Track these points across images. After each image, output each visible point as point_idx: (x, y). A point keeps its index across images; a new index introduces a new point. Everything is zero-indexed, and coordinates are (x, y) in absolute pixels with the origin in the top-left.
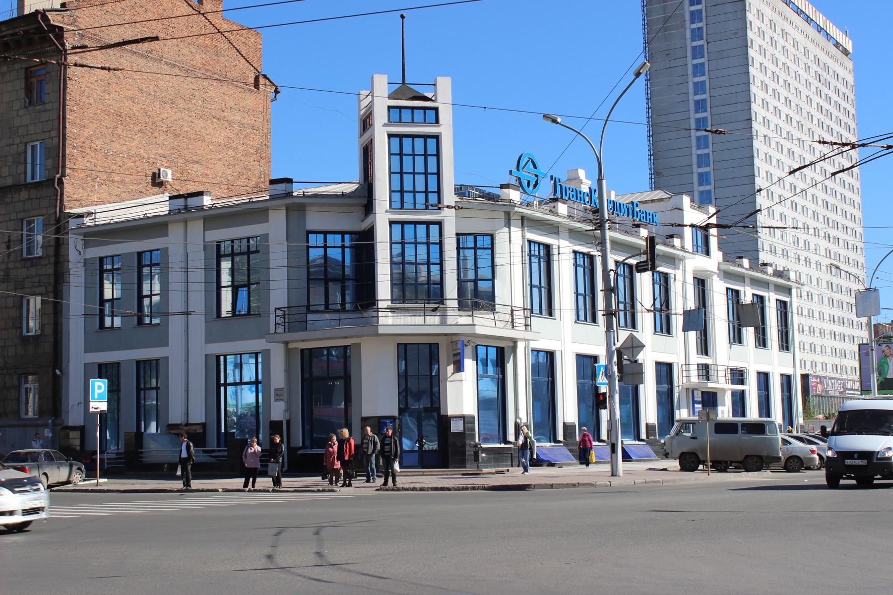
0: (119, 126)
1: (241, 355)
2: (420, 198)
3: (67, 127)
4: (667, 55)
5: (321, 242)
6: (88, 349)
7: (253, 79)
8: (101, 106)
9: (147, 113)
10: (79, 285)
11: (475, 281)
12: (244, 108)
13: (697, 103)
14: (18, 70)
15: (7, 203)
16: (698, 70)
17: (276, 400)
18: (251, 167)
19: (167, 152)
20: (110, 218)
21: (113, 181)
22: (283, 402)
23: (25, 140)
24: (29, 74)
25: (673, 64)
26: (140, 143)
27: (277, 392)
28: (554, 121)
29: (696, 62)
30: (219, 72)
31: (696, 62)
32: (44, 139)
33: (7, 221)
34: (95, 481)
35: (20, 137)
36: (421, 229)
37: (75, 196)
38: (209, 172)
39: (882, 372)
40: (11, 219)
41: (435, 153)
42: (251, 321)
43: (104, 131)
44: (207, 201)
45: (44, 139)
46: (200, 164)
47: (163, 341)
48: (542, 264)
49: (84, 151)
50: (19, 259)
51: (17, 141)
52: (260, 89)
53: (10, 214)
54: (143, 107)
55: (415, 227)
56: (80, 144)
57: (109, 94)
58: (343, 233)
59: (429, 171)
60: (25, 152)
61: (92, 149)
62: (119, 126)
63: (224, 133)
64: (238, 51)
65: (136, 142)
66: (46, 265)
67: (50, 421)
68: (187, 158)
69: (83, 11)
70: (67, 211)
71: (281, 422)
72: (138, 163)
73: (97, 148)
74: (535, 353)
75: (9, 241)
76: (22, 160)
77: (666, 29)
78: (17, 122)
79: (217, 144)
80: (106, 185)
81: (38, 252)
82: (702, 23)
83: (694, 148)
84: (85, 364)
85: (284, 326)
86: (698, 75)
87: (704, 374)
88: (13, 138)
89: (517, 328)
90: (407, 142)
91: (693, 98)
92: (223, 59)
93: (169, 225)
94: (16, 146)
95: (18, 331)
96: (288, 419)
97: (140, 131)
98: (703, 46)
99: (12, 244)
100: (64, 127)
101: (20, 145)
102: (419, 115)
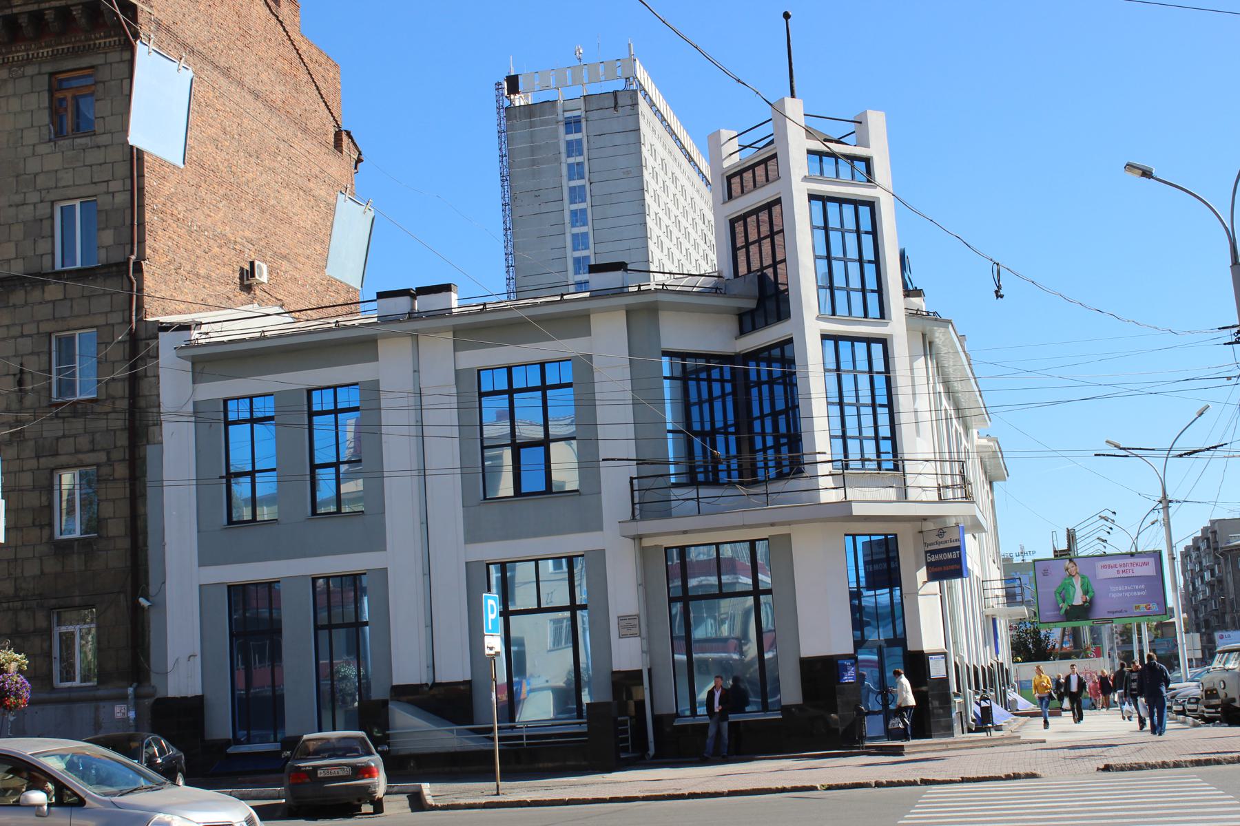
3: (146, 175)
4: (536, 196)
7: (333, 134)
10: (601, 403)
14: (32, 77)
15: (14, 306)
16: (578, 217)
17: (621, 636)
20: (260, 330)
21: (198, 275)
23: (52, 197)
24: (55, 85)
25: (544, 208)
27: (623, 623)
28: (1147, 174)
29: (574, 207)
31: (574, 207)
32: (95, 196)
33: (15, 338)
34: (493, 785)
35: (40, 191)
39: (1067, 596)
43: (187, 189)
44: (454, 300)
45: (95, 196)
47: (377, 542)
49: (165, 218)
50: (44, 403)
51: (33, 197)
52: (344, 153)
55: (853, 346)
60: (52, 217)
64: (318, 88)
65: (221, 214)
66: (107, 413)
67: (130, 690)
70: (149, 319)
71: (640, 672)
73: (179, 216)
75: (22, 372)
77: (534, 163)
78: (33, 166)
80: (190, 280)
81: (85, 388)
82: (582, 157)
84: (200, 586)
86: (578, 224)
88: (25, 193)
93: (379, 341)
94: (31, 207)
95: (46, 532)
97: (225, 196)
98: (584, 186)
99: (28, 378)
100: (141, 176)
101: (40, 206)
102: (845, 167)
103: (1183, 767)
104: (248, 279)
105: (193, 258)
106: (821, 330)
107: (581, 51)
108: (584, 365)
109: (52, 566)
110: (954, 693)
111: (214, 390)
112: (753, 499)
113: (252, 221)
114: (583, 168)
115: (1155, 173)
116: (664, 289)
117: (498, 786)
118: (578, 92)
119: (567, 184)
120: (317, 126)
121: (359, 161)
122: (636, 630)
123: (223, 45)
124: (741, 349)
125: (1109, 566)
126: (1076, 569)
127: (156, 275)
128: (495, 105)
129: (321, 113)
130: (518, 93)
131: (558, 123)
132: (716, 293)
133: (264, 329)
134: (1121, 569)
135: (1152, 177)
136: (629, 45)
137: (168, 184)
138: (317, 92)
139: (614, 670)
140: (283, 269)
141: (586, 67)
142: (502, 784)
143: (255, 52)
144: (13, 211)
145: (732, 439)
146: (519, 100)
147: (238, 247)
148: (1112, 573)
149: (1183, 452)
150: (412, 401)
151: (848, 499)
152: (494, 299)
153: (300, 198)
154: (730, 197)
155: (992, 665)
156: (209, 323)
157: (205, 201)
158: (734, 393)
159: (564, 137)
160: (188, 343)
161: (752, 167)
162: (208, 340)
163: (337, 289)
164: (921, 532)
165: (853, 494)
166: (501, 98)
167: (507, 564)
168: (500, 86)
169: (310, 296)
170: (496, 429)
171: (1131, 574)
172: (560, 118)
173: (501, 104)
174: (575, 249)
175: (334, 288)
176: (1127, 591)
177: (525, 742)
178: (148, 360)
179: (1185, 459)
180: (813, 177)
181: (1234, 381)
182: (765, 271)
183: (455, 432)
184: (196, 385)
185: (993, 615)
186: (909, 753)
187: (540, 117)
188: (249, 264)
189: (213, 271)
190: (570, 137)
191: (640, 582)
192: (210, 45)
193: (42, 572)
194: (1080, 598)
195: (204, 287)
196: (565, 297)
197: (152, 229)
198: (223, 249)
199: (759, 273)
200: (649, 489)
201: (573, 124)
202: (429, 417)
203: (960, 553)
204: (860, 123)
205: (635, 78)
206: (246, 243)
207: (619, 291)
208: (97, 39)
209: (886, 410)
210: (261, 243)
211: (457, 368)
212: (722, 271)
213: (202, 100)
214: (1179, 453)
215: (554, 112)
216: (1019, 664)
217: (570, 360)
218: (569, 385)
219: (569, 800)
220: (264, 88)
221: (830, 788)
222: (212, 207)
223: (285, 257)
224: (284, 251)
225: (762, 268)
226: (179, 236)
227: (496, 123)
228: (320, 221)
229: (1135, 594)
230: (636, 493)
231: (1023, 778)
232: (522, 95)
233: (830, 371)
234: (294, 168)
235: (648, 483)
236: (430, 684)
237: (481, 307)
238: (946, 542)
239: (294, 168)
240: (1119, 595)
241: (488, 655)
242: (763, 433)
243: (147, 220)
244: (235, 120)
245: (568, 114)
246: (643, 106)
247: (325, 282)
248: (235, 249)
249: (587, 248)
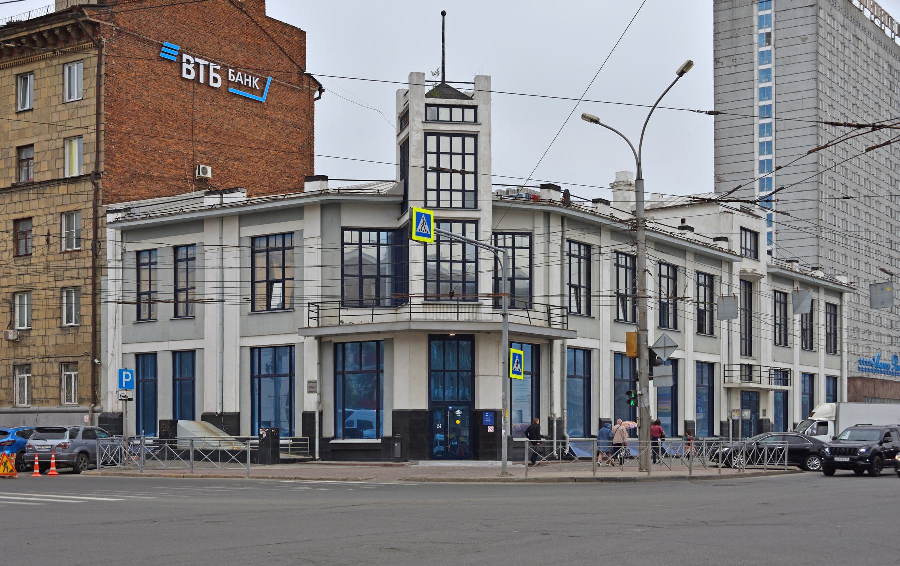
2: (458, 196)
5: (356, 239)
9: (187, 110)
11: (513, 280)
17: (309, 392)
18: (294, 165)
19: (207, 149)
20: (180, 209)
22: (316, 395)
27: (310, 385)
36: (457, 229)
37: (114, 191)
38: (250, 170)
40: (51, 213)
48: (582, 265)
50: (59, 252)
53: (49, 208)
54: (182, 104)
57: (148, 91)
58: (379, 231)
59: (467, 170)
62: (158, 123)
63: (266, 132)
68: (228, 155)
69: (121, 7)
71: (313, 414)
72: (177, 160)
74: (700, 365)
76: (61, 156)
79: (258, 142)
83: (757, 154)
85: (318, 320)
87: (748, 375)
89: (554, 327)
90: (445, 141)
92: (265, 58)
109: (61, 340)
110: (324, 441)
115: (601, 122)
116: (339, 192)
144: (47, 144)
193: (57, 344)
208: (83, 44)
220: (225, 56)
249: (770, 99)
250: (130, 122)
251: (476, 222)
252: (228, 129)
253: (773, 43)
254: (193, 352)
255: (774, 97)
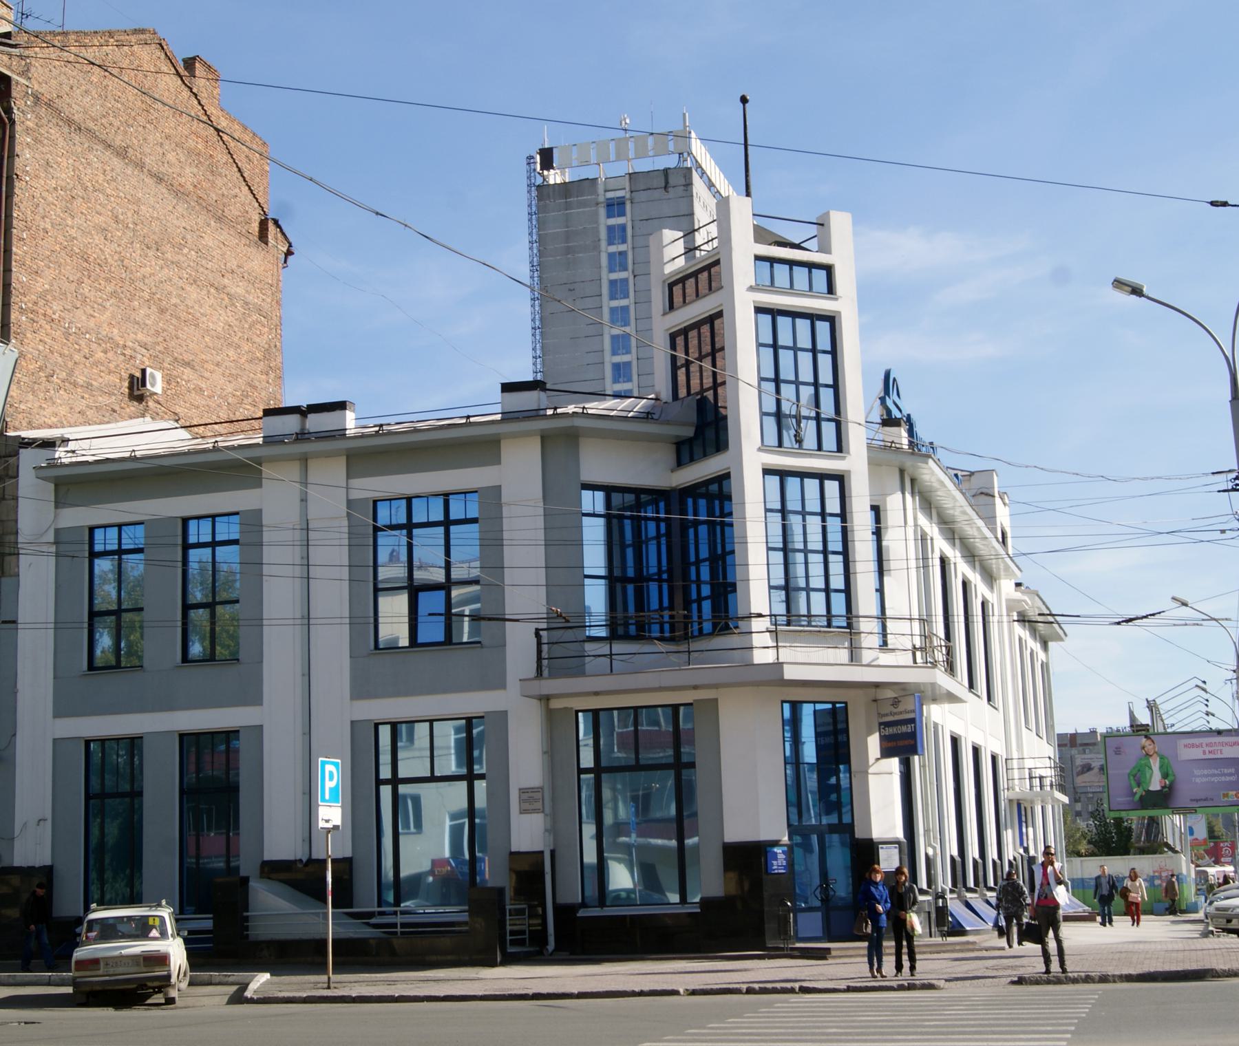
0: (86, 280)
1: (431, 722)
3: (14, 269)
4: (570, 290)
6: (61, 710)
8: (60, 238)
9: (122, 261)
12: (249, 274)
13: (616, 367)
17: (523, 811)
18: (257, 384)
20: (131, 449)
21: (75, 385)
26: (113, 317)
27: (525, 796)
28: (1137, 291)
30: (213, 202)
34: (324, 978)
41: (829, 349)
42: (208, 671)
44: (350, 421)
46: (193, 368)
47: (252, 695)
49: (36, 319)
52: (270, 245)
56: (30, 305)
57: (73, 217)
61: (47, 318)
62: (86, 280)
64: (240, 170)
65: (108, 314)
71: (542, 852)
72: (110, 355)
73: (53, 316)
77: (568, 250)
80: (65, 390)
91: (610, 359)
96: (552, 848)
97: (114, 294)
103: (1110, 982)
104: (138, 389)
105: (70, 364)
106: (763, 464)
107: (628, 121)
108: (491, 498)
111: (78, 517)
112: (673, 658)
113: (147, 322)
114: (626, 258)
117: (329, 978)
118: (622, 169)
119: (606, 276)
120: (238, 213)
121: (289, 253)
122: (539, 805)
123: (120, 121)
124: (680, 482)
125: (1193, 746)
126: (1154, 748)
127: (22, 383)
128: (525, 182)
129: (243, 199)
130: (553, 168)
131: (597, 204)
132: (647, 418)
133: (135, 448)
134: (1207, 749)
135: (1143, 296)
136: (684, 115)
137: (41, 280)
138: (239, 174)
139: (513, 850)
140: (185, 377)
141: (632, 139)
142: (334, 978)
143: (160, 129)
145: (665, 586)
146: (554, 177)
147: (128, 352)
148: (1197, 754)
149: (1120, 620)
150: (298, 535)
151: (781, 661)
152: (393, 420)
153: (211, 297)
154: (671, 307)
155: (1015, 859)
156: (76, 440)
157: (87, 300)
158: (668, 534)
159: (605, 222)
160: (50, 461)
161: (695, 274)
162: (74, 460)
163: (254, 401)
164: (875, 701)
165: (786, 655)
166: (532, 174)
167: (474, 720)
168: (532, 161)
169: (218, 409)
170: (392, 572)
171: (1219, 756)
172: (601, 199)
173: (533, 181)
174: (614, 353)
175: (250, 400)
176: (1214, 775)
177: (399, 930)
178: (7, 480)
179: (1124, 627)
180: (760, 287)
181: (1229, 534)
182: (705, 394)
183: (345, 573)
184: (59, 510)
185: (1018, 800)
186: (835, 957)
187: (577, 197)
188: (140, 371)
189: (95, 380)
190: (613, 221)
191: (545, 750)
192: (104, 121)
194: (1158, 783)
195: (83, 397)
196: (472, 420)
197: (19, 331)
198: (109, 354)
199: (699, 397)
200: (556, 643)
201: (616, 207)
202: (316, 555)
203: (915, 727)
204: (822, 225)
205: (690, 153)
206: (139, 347)
207: (534, 413)
209: (840, 558)
210: (158, 348)
211: (350, 498)
212: (660, 393)
213: (89, 184)
214: (1117, 620)
215: (595, 192)
216: (1082, 858)
217: (476, 492)
218: (474, 521)
219: (399, 996)
220: (170, 170)
221: (694, 993)
222: (96, 306)
223: (189, 363)
224: (188, 357)
225: (703, 390)
226: (53, 339)
227: (526, 203)
228: (237, 323)
229: (1223, 779)
230: (545, 648)
231: (919, 989)
232: (558, 171)
233: (772, 511)
234: (204, 262)
235: (557, 635)
236: (305, 860)
237: (377, 429)
238: (901, 713)
239: (204, 262)
240: (1205, 780)
241: (322, 828)
242: (699, 582)
243: (12, 320)
244: (130, 206)
245: (610, 195)
246: (698, 186)
247: (238, 393)
248: (124, 355)
249: (628, 352)
250: (47, 272)
251: (841, 478)
252: (175, 305)
253: (630, 267)
254: (230, 735)
255: (634, 350)
